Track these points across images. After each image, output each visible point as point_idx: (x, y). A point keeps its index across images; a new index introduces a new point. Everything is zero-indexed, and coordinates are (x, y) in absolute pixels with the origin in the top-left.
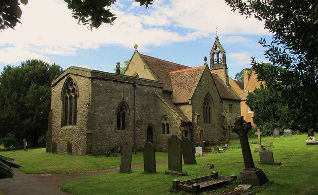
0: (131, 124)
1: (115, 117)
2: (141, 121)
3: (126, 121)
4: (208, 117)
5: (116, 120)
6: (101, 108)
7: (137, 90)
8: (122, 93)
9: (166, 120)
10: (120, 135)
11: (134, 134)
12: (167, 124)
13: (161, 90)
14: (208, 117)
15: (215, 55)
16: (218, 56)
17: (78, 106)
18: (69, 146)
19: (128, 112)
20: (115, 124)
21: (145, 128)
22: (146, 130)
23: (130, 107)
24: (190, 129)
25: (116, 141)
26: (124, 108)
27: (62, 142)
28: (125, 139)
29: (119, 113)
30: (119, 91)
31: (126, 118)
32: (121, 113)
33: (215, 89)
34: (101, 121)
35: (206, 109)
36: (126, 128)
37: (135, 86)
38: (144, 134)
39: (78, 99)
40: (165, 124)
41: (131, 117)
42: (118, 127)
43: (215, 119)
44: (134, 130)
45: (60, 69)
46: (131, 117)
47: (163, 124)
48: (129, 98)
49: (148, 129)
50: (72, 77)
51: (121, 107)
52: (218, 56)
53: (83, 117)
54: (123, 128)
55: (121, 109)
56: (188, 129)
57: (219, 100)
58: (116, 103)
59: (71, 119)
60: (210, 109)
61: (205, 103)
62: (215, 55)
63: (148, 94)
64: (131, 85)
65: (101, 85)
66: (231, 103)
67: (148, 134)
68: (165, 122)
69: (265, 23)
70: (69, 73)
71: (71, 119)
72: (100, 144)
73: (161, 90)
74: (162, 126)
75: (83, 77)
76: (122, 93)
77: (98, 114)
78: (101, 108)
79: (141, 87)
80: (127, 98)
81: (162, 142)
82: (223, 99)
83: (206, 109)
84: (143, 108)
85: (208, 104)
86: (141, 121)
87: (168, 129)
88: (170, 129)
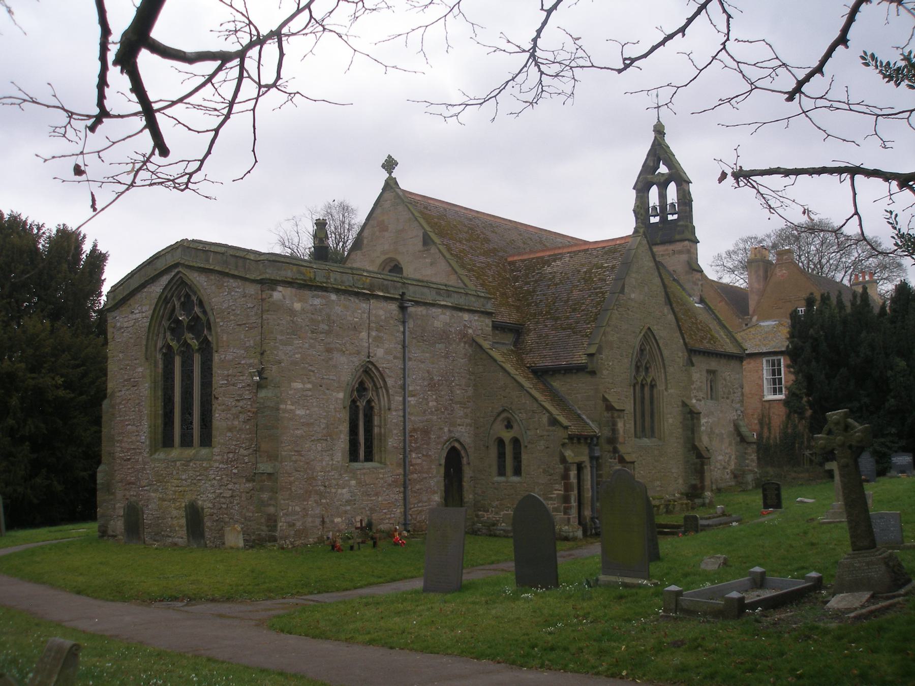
0: (393, 441)
1: (345, 415)
2: (426, 432)
3: (376, 430)
4: (648, 419)
5: (345, 428)
6: (298, 385)
7: (410, 324)
8: (364, 335)
9: (509, 426)
10: (359, 483)
11: (405, 475)
12: (516, 442)
13: (488, 321)
14: (648, 419)
15: (654, 192)
16: (663, 196)
17: (218, 380)
18: (195, 520)
19: (384, 402)
20: (342, 442)
21: (439, 454)
22: (443, 462)
23: (390, 382)
24: (592, 458)
25: (348, 502)
26: (369, 385)
27: (164, 506)
28: (377, 494)
29: (354, 402)
30: (355, 328)
31: (376, 420)
32: (362, 404)
33: (671, 317)
34: (299, 432)
35: (643, 386)
36: (376, 457)
37: (403, 308)
38: (436, 480)
39: (216, 357)
40: (507, 442)
41: (394, 417)
42: (353, 455)
43: (670, 420)
44: (404, 463)
45: (87, 248)
46: (394, 417)
47: (501, 442)
48: (388, 352)
49: (447, 458)
50: (199, 280)
51: (362, 384)
52: (663, 196)
53: (236, 416)
54: (369, 458)
55: (361, 388)
56: (585, 459)
57: (681, 356)
58: (346, 368)
59: (187, 424)
60: (652, 386)
61: (638, 368)
62: (654, 192)
63: (444, 336)
64: (393, 307)
65: (297, 306)
66: (714, 364)
67: (447, 475)
68: (507, 436)
69: (119, 68)
70: (176, 265)
71: (187, 424)
72: (297, 509)
73: (488, 321)
74: (494, 452)
75: (234, 277)
76: (364, 335)
77: (289, 407)
78: (298, 385)
79: (420, 310)
80: (380, 352)
81: (496, 503)
82: (692, 352)
83: (643, 386)
84: (432, 386)
85: (647, 369)
86: (426, 432)
87: (517, 458)
88: (524, 457)
